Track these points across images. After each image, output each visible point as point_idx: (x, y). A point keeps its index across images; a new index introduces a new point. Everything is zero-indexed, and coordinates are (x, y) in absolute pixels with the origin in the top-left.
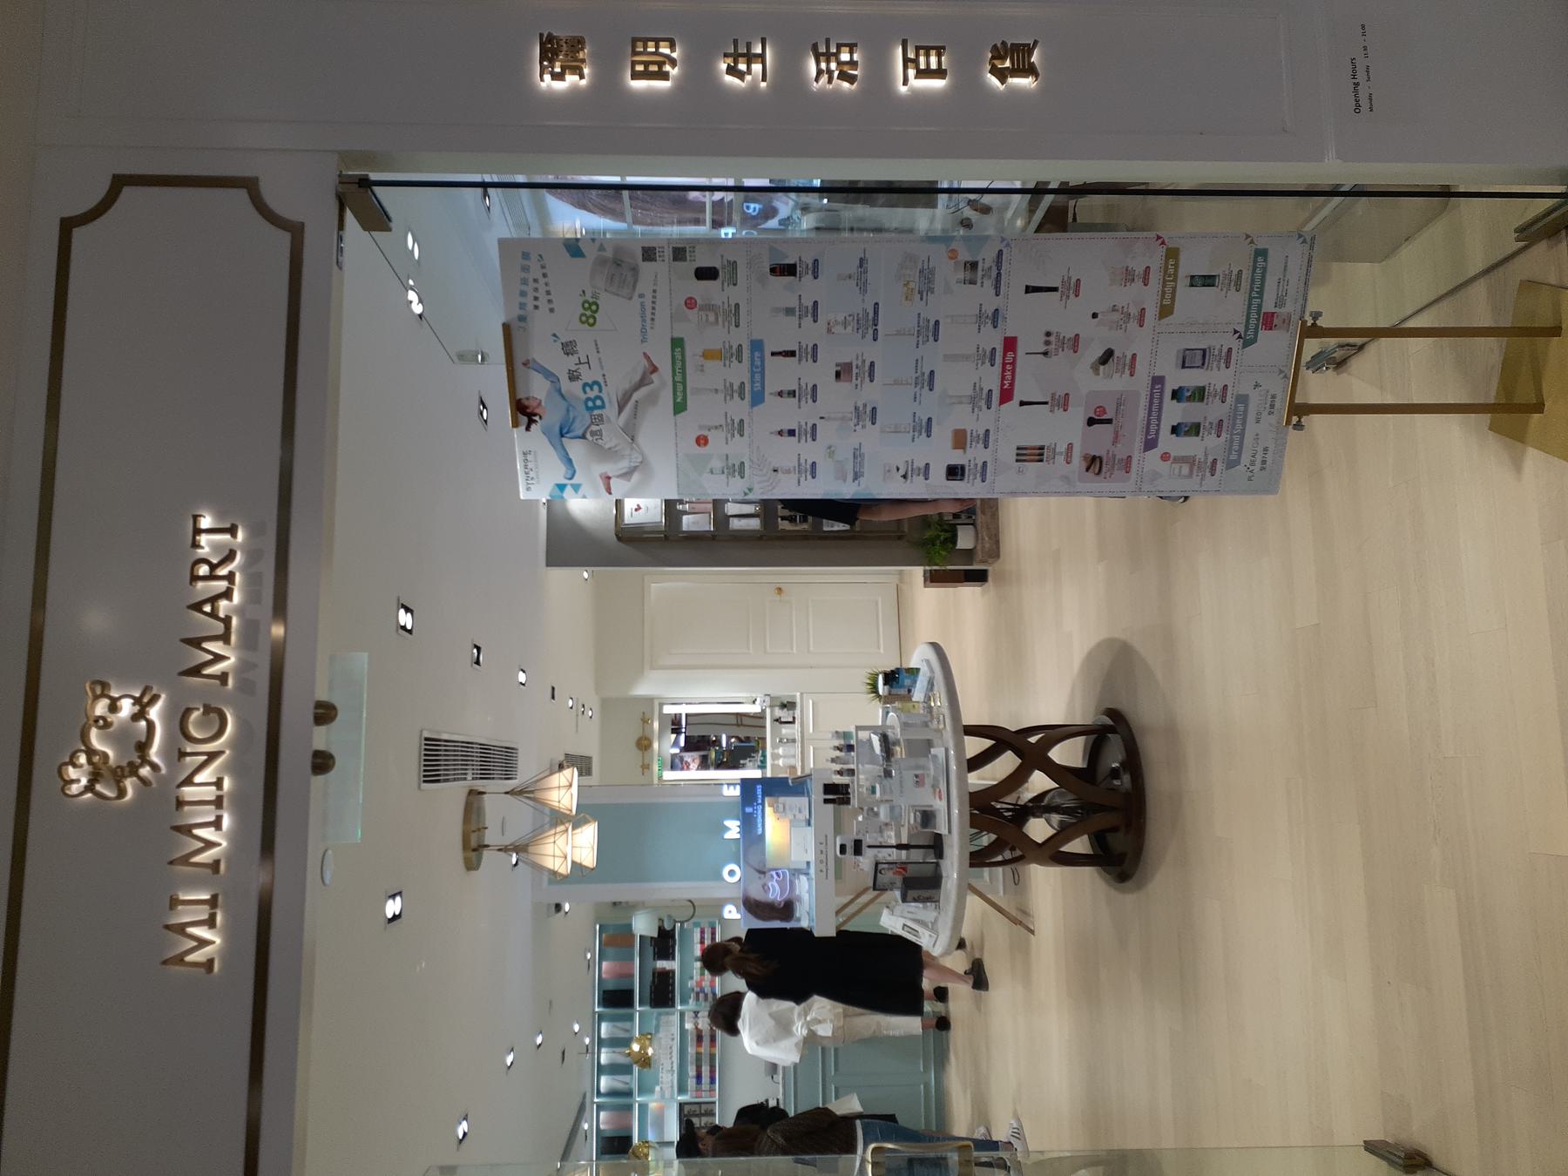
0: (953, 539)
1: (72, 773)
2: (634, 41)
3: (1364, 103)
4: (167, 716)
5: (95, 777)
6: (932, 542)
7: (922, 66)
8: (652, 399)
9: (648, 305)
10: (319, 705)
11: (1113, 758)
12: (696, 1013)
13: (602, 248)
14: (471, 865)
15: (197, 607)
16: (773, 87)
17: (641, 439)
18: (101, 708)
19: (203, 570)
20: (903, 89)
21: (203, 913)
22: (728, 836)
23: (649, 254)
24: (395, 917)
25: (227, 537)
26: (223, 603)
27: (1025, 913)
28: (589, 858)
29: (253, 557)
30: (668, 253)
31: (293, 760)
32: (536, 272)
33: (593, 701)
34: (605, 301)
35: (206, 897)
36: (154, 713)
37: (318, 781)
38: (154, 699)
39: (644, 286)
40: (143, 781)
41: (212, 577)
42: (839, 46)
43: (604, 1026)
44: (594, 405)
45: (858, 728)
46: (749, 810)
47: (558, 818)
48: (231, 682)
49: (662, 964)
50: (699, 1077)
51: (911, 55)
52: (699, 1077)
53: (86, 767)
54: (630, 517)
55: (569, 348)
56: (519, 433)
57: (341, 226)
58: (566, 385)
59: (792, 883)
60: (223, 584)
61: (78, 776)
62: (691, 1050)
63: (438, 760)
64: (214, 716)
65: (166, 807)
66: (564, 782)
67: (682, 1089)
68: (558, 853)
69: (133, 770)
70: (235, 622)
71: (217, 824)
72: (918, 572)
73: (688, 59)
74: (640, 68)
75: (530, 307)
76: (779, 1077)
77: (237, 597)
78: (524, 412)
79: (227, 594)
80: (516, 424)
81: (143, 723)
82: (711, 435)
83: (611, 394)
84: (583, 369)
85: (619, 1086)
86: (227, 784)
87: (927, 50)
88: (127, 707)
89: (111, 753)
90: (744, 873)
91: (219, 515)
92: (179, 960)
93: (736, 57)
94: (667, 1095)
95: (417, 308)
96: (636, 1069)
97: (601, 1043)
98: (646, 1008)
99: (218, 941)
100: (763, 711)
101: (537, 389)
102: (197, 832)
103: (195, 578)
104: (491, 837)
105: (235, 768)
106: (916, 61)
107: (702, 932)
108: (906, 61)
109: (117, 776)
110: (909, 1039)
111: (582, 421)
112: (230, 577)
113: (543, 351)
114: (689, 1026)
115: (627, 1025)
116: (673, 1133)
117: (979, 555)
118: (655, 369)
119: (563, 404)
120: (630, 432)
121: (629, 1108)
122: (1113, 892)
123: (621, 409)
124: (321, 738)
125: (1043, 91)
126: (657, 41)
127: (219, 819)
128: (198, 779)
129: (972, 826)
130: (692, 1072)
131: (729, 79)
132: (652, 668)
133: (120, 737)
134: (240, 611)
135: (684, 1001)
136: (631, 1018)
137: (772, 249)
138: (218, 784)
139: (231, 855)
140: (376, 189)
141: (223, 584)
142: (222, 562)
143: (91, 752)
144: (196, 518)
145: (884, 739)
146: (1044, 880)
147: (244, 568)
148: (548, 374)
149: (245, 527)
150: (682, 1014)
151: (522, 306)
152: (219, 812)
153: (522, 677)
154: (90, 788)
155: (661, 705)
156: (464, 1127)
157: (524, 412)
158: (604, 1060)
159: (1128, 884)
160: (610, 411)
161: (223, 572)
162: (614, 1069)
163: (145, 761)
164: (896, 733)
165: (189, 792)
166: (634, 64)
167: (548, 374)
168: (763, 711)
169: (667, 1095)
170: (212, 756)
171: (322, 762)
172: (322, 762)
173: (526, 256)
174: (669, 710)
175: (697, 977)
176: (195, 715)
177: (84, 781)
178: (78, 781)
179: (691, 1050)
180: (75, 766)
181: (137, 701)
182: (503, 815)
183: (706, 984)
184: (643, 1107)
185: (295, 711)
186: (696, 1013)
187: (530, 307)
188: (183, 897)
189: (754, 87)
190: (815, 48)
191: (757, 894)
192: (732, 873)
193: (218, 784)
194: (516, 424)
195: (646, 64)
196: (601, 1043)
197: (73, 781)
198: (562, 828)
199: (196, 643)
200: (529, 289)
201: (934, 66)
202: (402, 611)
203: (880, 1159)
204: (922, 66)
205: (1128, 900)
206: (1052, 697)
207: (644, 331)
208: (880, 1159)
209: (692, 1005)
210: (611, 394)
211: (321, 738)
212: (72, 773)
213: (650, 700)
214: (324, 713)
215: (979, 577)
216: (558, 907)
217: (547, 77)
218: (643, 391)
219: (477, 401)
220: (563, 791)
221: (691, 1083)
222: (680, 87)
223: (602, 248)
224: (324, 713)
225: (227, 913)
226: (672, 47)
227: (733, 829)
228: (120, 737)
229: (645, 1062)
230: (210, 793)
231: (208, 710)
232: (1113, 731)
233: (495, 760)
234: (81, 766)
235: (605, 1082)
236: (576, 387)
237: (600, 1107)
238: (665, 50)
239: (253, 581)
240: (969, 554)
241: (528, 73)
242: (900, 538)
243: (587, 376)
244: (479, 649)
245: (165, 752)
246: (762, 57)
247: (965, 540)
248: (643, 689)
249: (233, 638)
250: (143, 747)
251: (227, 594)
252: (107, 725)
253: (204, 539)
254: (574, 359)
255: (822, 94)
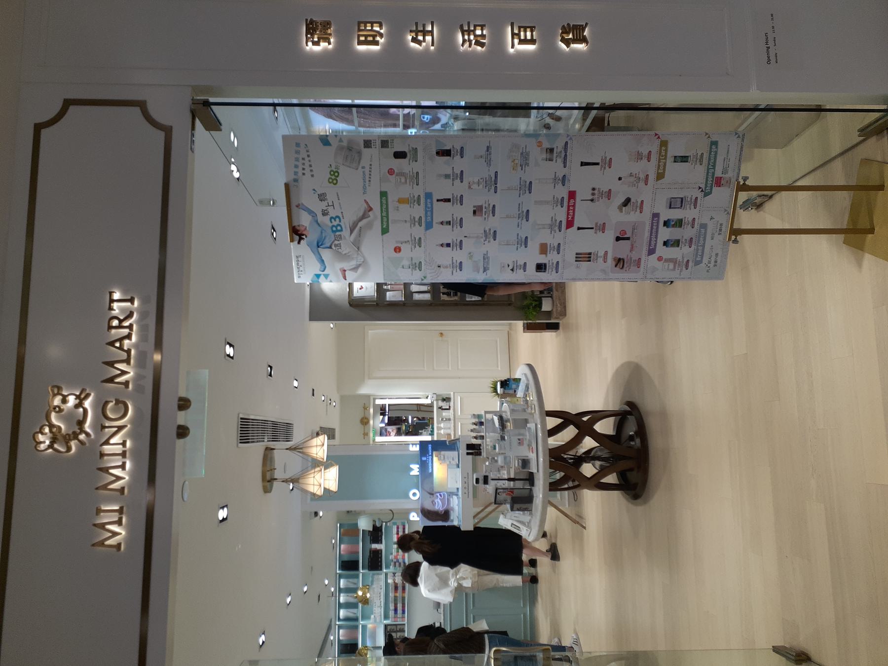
0: (540, 305)
1: (41, 438)
2: (359, 23)
3: (773, 58)
4: (95, 405)
5: (54, 440)
6: (528, 307)
7: (522, 38)
8: (369, 226)
9: (367, 173)
10: (181, 399)
11: (631, 429)
12: (394, 574)
13: (341, 141)
14: (267, 490)
15: (112, 344)
16: (438, 49)
17: (363, 249)
18: (57, 401)
19: (115, 323)
20: (511, 51)
21: (115, 517)
22: (412, 473)
23: (368, 144)
24: (224, 519)
25: (129, 304)
26: (126, 342)
27: (581, 517)
28: (333, 486)
29: (143, 315)
30: (378, 144)
31: (166, 430)
32: (303, 154)
33: (336, 397)
34: (343, 170)
35: (117, 508)
36: (87, 404)
37: (180, 442)
38: (87, 396)
39: (365, 162)
40: (81, 442)
41: (120, 327)
42: (475, 26)
43: (342, 581)
44: (336, 229)
45: (486, 412)
46: (424, 459)
47: (316, 463)
48: (131, 386)
49: (375, 546)
50: (396, 610)
51: (516, 31)
52: (396, 610)
53: (49, 434)
54: (357, 293)
55: (322, 197)
56: (294, 245)
57: (193, 128)
58: (320, 218)
59: (448, 500)
60: (127, 331)
61: (44, 439)
62: (391, 595)
63: (248, 430)
64: (121, 405)
65: (94, 457)
66: (319, 443)
67: (386, 617)
68: (316, 483)
69: (75, 436)
70: (133, 352)
71: (123, 467)
72: (520, 324)
73: (390, 34)
74: (362, 38)
75: (300, 174)
76: (441, 610)
77: (134, 338)
78: (297, 233)
79: (129, 337)
80: (292, 240)
81: (81, 410)
82: (403, 247)
83: (346, 223)
84: (330, 209)
85: (351, 615)
86: (128, 444)
87: (525, 29)
88: (72, 401)
89: (63, 426)
90: (421, 495)
91: (124, 292)
92: (102, 544)
93: (417, 32)
94: (378, 620)
95: (236, 175)
96: (360, 605)
97: (340, 591)
98: (366, 571)
99: (124, 533)
100: (432, 403)
101: (304, 220)
102: (111, 471)
103: (111, 327)
104: (278, 474)
105: (133, 435)
106: (519, 35)
107: (398, 528)
108: (513, 34)
109: (66, 440)
110: (515, 588)
111: (329, 238)
112: (130, 327)
113: (308, 199)
114: (390, 581)
115: (355, 580)
116: (381, 641)
117: (555, 314)
118: (371, 209)
119: (319, 229)
120: (357, 244)
121: (356, 627)
122: (630, 505)
123: (351, 232)
124: (182, 418)
125: (591, 51)
126: (372, 23)
127: (124, 464)
128: (112, 441)
129: (550, 468)
130: (392, 607)
131: (413, 45)
132: (369, 378)
133: (68, 418)
134: (136, 346)
135: (387, 567)
136: (357, 577)
137: (437, 141)
138: (124, 444)
139: (131, 484)
140: (213, 107)
141: (127, 331)
142: (126, 319)
143: (51, 426)
144: (111, 293)
145: (501, 418)
146: (591, 498)
147: (138, 322)
148: (310, 212)
149: (139, 299)
150: (386, 574)
151: (296, 173)
152: (124, 460)
153: (296, 384)
154: (51, 446)
155: (374, 399)
156: (263, 638)
157: (297, 233)
158: (342, 600)
159: (639, 501)
160: (346, 233)
161: (126, 324)
162: (348, 605)
163: (82, 431)
164: (507, 415)
165: (107, 449)
166: (359, 36)
167: (310, 212)
168: (432, 403)
169: (378, 620)
170: (120, 428)
171: (182, 432)
172: (182, 432)
173: (298, 145)
174: (379, 402)
175: (394, 553)
176: (110, 405)
177: (48, 442)
178: (44, 442)
179: (391, 595)
180: (42, 434)
181: (78, 397)
182: (285, 461)
183: (400, 557)
184: (364, 627)
185: (167, 403)
186: (394, 574)
187: (300, 174)
188: (104, 508)
189: (427, 49)
190: (461, 27)
191: (428, 506)
192: (415, 495)
193: (124, 444)
194: (292, 240)
195: (366, 36)
196: (340, 591)
197: (41, 443)
198: (318, 469)
199: (111, 364)
200: (300, 164)
201: (529, 37)
202: (228, 346)
203: (498, 656)
204: (522, 38)
205: (639, 510)
206: (596, 395)
207: (364, 188)
208: (498, 656)
209: (392, 569)
210: (346, 223)
211: (182, 418)
212: (41, 438)
213: (368, 397)
214: (184, 404)
215: (554, 327)
216: (316, 514)
217: (310, 44)
218: (364, 221)
219: (270, 227)
220: (319, 448)
221: (392, 613)
222: (385, 49)
223: (341, 141)
224: (184, 404)
225: (128, 517)
226: (381, 27)
227: (415, 469)
228: (68, 418)
229: (365, 601)
230: (119, 449)
231: (118, 402)
232: (630, 414)
233: (280, 431)
234: (46, 434)
235: (343, 613)
236: (326, 219)
237: (340, 627)
238: (377, 28)
239: (143, 329)
240: (549, 314)
241: (299, 42)
242: (510, 305)
243: (332, 213)
244: (271, 367)
245: (93, 426)
246: (431, 32)
247: (546, 306)
248: (364, 390)
249: (132, 361)
250: (81, 423)
251: (129, 337)
252: (61, 410)
253: (115, 305)
254: (325, 203)
255: (466, 53)
